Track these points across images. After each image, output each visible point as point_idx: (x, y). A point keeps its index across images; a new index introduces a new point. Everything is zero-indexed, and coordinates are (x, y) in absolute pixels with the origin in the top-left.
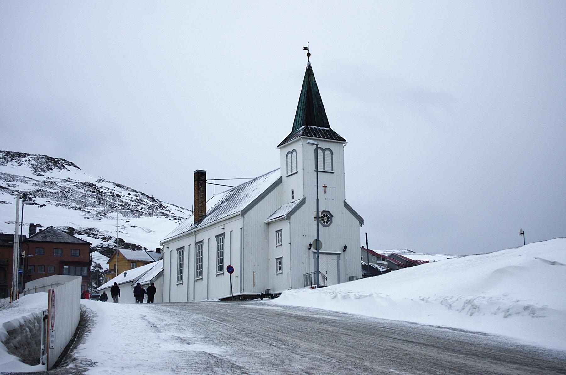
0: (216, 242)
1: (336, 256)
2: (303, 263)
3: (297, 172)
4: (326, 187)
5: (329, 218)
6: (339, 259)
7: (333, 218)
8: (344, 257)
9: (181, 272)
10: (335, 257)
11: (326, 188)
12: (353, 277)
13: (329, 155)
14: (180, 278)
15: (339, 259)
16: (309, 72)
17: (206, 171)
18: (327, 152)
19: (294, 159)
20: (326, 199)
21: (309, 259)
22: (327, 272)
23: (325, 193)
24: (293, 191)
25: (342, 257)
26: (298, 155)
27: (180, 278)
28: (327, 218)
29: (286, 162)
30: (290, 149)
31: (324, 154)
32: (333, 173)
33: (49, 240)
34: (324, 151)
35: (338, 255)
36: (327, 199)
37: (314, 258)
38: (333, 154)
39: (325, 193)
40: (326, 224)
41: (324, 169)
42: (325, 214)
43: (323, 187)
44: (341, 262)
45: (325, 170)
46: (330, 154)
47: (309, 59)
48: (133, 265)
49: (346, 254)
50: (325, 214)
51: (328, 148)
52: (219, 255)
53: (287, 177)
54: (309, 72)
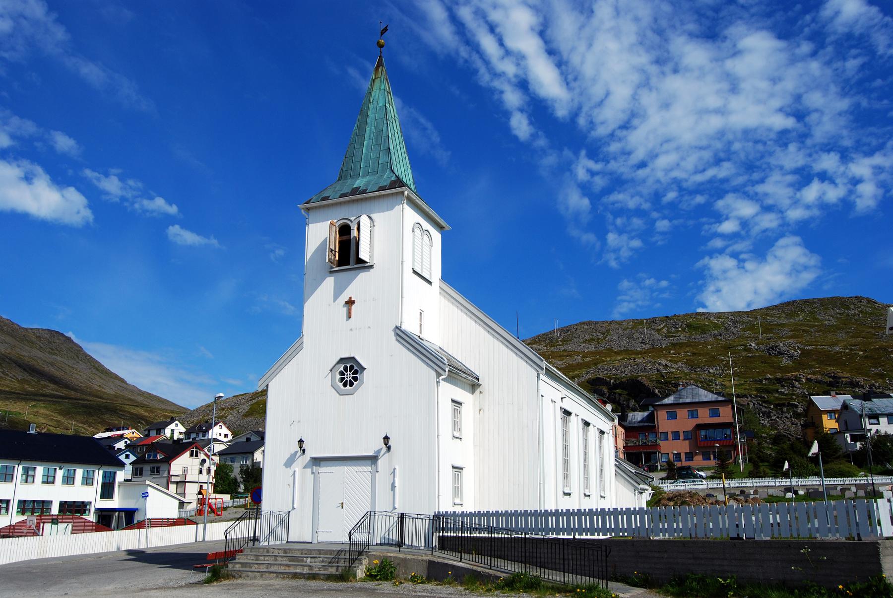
4: (353, 302)
5: (356, 381)
11: (354, 307)
20: (351, 330)
33: (681, 401)
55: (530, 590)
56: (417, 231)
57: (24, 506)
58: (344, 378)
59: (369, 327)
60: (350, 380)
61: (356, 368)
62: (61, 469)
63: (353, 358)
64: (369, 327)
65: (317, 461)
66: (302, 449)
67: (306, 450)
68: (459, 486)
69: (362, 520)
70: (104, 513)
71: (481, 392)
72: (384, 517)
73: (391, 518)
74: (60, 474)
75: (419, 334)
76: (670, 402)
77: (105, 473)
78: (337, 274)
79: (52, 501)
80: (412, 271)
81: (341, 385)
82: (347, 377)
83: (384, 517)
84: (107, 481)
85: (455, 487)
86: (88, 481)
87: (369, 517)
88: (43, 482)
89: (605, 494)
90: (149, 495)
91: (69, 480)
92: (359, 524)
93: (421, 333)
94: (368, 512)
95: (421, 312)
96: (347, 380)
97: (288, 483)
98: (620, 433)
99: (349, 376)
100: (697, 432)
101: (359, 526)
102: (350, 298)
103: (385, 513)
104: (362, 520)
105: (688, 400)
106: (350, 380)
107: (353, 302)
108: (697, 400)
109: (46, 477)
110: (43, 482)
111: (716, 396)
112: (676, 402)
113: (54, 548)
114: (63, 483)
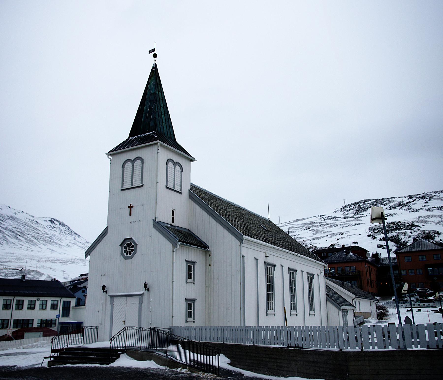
0: (265, 270)
1: (138, 298)
2: (98, 311)
3: (142, 186)
4: (133, 207)
5: (132, 252)
6: (141, 303)
7: (138, 246)
8: (149, 298)
9: (311, 300)
10: (137, 299)
11: (132, 209)
12: (143, 329)
13: (177, 177)
14: (312, 308)
15: (141, 303)
16: (154, 74)
17: (50, 310)
18: (178, 168)
19: (138, 172)
20: (131, 223)
21: (106, 305)
22: (124, 321)
23: (130, 215)
24: (173, 212)
25: (145, 298)
26: (144, 164)
27: (312, 308)
28: (127, 248)
29: (183, 178)
30: (132, 155)
31: (175, 168)
32: (181, 193)
34: (175, 164)
35: (141, 297)
36: (132, 223)
37: (110, 304)
38: (183, 172)
39: (130, 215)
40: (129, 255)
41: (174, 188)
42: (129, 243)
43: (129, 207)
44: (144, 306)
45: (175, 188)
46: (180, 171)
47: (155, 61)
48: (23, 322)
49: (151, 295)
50: (129, 243)
51: (179, 163)
52: (294, 282)
53: (122, 190)
54: (154, 74)
55: (165, 374)
56: (171, 164)
57: (17, 322)
58: (127, 250)
59: (140, 221)
60: (130, 251)
61: (133, 244)
62: (38, 300)
63: (125, 240)
64: (140, 221)
65: (111, 297)
66: (105, 291)
67: (108, 291)
68: (192, 310)
69: (121, 332)
70: (63, 325)
71: (210, 255)
72: (134, 330)
73: (93, 329)
74: (38, 304)
75: (170, 222)
76: (407, 251)
77: (64, 302)
78: (137, 189)
79: (33, 320)
80: (165, 187)
81: (125, 254)
82: (128, 250)
83: (134, 330)
84: (66, 306)
85: (310, 305)
86: (54, 307)
87: (126, 330)
88: (28, 308)
89: (297, 312)
90: (56, 316)
91: (43, 307)
92: (119, 334)
93: (173, 221)
94: (125, 327)
95: (174, 210)
96: (128, 251)
97: (98, 310)
98: (373, 270)
99: (129, 249)
100: (242, 325)
101: (120, 334)
102: (106, 154)
103: (134, 328)
104: (121, 332)
105: (419, 249)
106: (130, 251)
107: (133, 207)
108: (425, 249)
109: (30, 305)
110: (28, 308)
111: (438, 246)
112: (411, 250)
113: (131, 339)
114: (51, 309)
